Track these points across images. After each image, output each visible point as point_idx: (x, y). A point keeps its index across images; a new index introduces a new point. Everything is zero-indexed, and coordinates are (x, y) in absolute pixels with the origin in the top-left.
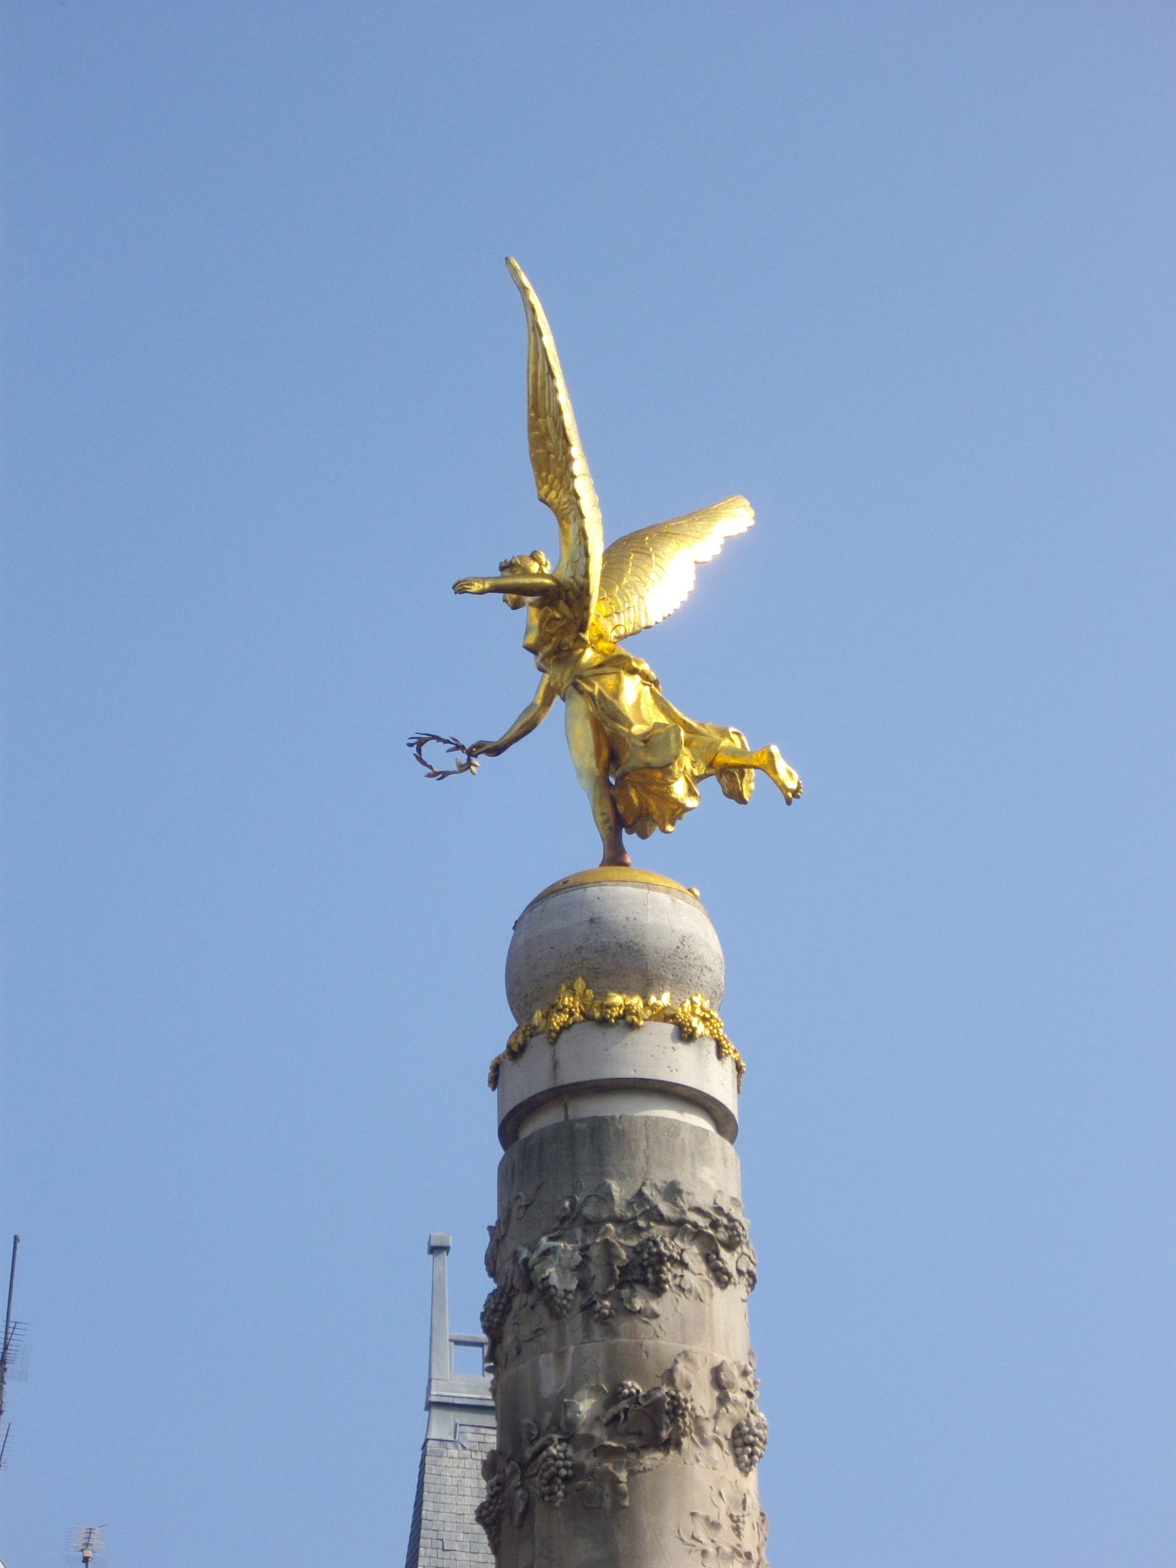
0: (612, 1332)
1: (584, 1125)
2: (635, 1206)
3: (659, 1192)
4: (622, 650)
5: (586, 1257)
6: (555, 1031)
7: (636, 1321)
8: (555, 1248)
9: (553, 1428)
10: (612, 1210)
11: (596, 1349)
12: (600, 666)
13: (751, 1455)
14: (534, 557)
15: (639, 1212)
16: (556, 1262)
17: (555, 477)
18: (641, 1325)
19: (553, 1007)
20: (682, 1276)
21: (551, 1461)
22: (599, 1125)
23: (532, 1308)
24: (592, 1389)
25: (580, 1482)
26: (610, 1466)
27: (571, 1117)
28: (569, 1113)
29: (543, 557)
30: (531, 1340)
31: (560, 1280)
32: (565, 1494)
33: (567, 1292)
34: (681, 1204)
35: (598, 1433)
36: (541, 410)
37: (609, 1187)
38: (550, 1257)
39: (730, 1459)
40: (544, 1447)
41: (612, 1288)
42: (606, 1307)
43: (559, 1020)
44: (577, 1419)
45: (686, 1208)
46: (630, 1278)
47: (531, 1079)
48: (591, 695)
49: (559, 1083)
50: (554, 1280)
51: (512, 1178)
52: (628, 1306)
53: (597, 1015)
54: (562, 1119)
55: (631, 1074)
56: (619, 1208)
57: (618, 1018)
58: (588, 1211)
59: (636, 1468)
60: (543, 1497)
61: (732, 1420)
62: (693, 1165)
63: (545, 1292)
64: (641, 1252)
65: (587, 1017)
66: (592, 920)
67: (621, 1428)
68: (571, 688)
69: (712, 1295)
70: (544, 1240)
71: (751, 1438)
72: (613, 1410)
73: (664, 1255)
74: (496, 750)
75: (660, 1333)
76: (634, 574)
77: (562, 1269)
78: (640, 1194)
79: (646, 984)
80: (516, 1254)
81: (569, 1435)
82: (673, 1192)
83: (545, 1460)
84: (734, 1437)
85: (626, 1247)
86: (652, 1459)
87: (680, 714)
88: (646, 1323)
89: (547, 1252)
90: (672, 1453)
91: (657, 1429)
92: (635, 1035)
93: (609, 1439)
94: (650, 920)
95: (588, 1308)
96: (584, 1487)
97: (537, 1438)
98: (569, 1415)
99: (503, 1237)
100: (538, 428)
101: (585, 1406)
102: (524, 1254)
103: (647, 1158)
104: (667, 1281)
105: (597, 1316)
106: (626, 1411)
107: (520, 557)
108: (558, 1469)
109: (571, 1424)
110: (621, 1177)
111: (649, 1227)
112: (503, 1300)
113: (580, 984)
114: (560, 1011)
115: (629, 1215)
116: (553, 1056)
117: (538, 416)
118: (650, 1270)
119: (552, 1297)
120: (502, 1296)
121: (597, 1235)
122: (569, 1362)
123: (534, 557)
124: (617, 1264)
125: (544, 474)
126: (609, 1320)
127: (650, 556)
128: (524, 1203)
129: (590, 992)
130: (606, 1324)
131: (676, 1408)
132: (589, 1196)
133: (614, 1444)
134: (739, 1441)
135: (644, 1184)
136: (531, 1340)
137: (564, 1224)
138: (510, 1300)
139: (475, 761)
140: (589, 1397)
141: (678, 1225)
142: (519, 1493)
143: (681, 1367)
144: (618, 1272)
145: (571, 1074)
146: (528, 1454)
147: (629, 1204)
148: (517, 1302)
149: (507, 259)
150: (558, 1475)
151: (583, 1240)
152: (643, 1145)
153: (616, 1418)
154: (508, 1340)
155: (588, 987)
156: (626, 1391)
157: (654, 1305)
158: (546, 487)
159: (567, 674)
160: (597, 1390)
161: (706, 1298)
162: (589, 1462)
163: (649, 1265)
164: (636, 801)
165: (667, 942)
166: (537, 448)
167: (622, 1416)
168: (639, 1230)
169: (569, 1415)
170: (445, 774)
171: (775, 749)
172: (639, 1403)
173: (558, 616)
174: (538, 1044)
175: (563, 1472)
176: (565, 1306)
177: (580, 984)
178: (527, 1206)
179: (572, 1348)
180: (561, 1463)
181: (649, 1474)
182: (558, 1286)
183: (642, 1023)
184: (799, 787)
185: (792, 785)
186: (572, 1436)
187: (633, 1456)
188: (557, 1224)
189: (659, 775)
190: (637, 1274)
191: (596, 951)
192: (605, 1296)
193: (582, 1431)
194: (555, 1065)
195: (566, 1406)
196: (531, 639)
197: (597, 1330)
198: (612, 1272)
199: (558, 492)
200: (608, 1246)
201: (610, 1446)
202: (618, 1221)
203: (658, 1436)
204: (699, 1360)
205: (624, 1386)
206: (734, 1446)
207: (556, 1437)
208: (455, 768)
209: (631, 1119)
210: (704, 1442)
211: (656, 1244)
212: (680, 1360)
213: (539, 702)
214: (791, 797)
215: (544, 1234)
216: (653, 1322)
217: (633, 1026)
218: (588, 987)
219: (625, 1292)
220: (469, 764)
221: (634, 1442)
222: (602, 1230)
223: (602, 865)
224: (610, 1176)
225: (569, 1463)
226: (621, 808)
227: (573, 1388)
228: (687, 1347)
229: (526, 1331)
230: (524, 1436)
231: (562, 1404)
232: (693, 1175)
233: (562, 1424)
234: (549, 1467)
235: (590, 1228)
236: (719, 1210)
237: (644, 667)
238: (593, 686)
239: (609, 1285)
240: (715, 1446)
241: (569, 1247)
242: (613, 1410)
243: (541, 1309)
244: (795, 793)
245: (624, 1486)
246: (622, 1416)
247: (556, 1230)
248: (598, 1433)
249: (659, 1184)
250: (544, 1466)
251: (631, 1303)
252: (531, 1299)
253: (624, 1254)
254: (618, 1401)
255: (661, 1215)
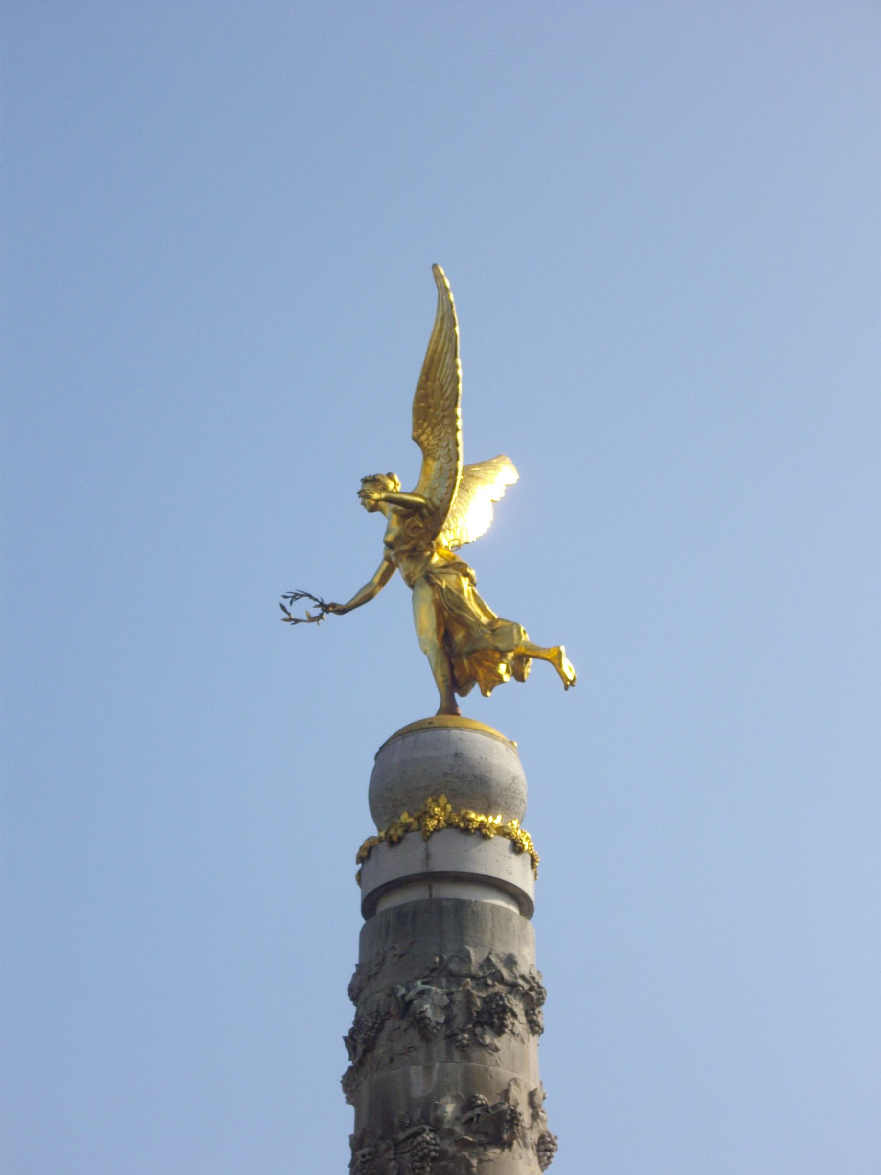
0: (467, 1058)
1: (449, 904)
2: (485, 968)
3: (501, 960)
4: (460, 558)
5: (452, 1001)
6: (429, 831)
7: (484, 1052)
8: (429, 990)
9: (423, 1121)
10: (470, 969)
11: (456, 1068)
12: (445, 567)
13: (549, 1158)
14: (390, 476)
15: (488, 973)
16: (430, 1001)
17: (428, 426)
18: (488, 1055)
19: (425, 813)
20: (513, 1024)
21: (425, 1145)
22: (460, 906)
23: (405, 1030)
24: (454, 1097)
25: (443, 1163)
26: (467, 1154)
27: (434, 896)
28: (434, 893)
29: (396, 478)
30: (403, 1054)
31: (433, 1015)
32: (432, 1169)
33: (437, 1023)
34: (515, 971)
35: (458, 1129)
36: (431, 377)
37: (468, 952)
38: (425, 996)
39: (536, 1159)
40: (416, 1135)
41: (470, 1026)
42: (465, 1039)
43: (432, 824)
44: (443, 1118)
45: (518, 975)
46: (482, 1020)
47: (395, 864)
48: (441, 587)
49: (430, 870)
50: (429, 1014)
51: (387, 933)
52: (481, 1040)
53: (462, 825)
54: (427, 897)
55: (483, 872)
56: (474, 969)
57: (476, 829)
58: (453, 967)
59: (484, 1158)
60: (414, 1169)
61: (539, 1131)
62: (519, 944)
63: (420, 1022)
64: (491, 1002)
65: (450, 825)
66: (456, 755)
67: (474, 1127)
68: (423, 580)
69: (529, 1040)
70: (419, 982)
71: (551, 1146)
72: (469, 1114)
73: (507, 1007)
74: (342, 611)
75: (500, 1063)
76: (460, 503)
77: (434, 1006)
78: (488, 960)
79: (488, 808)
80: (393, 992)
81: (437, 1126)
82: (511, 961)
83: (419, 1144)
84: (539, 1144)
85: (479, 997)
86: (494, 1152)
87: (490, 611)
88: (491, 1054)
89: (422, 993)
90: (506, 1150)
91: (499, 1133)
92: (485, 844)
93: (467, 1134)
94: (495, 761)
95: (451, 1038)
96: (446, 1167)
97: (409, 1127)
98: (439, 1113)
99: (375, 974)
100: (425, 389)
101: (450, 1108)
102: (402, 991)
103: (493, 935)
104: (506, 1026)
105: (458, 1044)
106: (478, 1115)
107: (382, 476)
108: (430, 1151)
109: (439, 1120)
110: (475, 946)
111: (494, 985)
112: (379, 1021)
113: (443, 800)
114: (432, 817)
115: (481, 974)
116: (426, 849)
117: (427, 380)
118: (496, 1016)
119: (426, 1026)
120: (377, 1018)
121: (460, 986)
122: (435, 1075)
123: (390, 476)
124: (474, 1008)
125: (421, 421)
126: (466, 1049)
127: (467, 491)
128: (399, 952)
129: (449, 807)
130: (464, 1051)
131: (513, 1118)
132: (452, 956)
133: (471, 1139)
134: (542, 1147)
135: (490, 953)
136: (403, 1054)
137: (434, 973)
138: (383, 1022)
139: (325, 615)
140: (452, 1103)
141: (513, 987)
142: (393, 1164)
143: (513, 1088)
144: (475, 1014)
145: (440, 865)
146: (401, 1136)
147: (481, 967)
148: (389, 1024)
149: (435, 267)
150: (428, 1155)
151: (448, 988)
152: (490, 924)
153: (470, 1120)
154: (380, 1051)
155: (448, 802)
156: (479, 1102)
157: (497, 1042)
158: (420, 431)
159: (419, 568)
160: (456, 1098)
161: (526, 1041)
162: (452, 1150)
163: (495, 1013)
164: (467, 669)
165: (506, 780)
166: (421, 402)
167: (475, 1119)
168: (487, 986)
169: (439, 1113)
170: (296, 621)
171: (563, 649)
172: (488, 1112)
173: (421, 525)
174: (413, 840)
175: (433, 1154)
176: (434, 1033)
177: (443, 800)
178: (401, 956)
179: (437, 1065)
180: (432, 1147)
181: (491, 1163)
182: (432, 1018)
183: (492, 836)
184: (574, 679)
185: (571, 677)
186: (439, 1129)
187: (481, 1149)
188: (427, 973)
189: (497, 655)
190: (486, 1018)
191: (458, 778)
192: (463, 1031)
193: (446, 1126)
194: (428, 856)
195: (436, 1107)
196: (390, 538)
197: (457, 1055)
198: (471, 1014)
199: (428, 436)
200: (468, 995)
201: (467, 1140)
202: (473, 977)
203: (501, 1138)
204: (522, 1084)
205: (477, 1098)
206: (538, 1150)
207: (427, 1128)
208: (305, 618)
209: (483, 904)
210: (525, 1145)
211: (502, 998)
212: (512, 1084)
213: (376, 580)
214: (569, 684)
215: (417, 978)
216: (496, 1054)
217: (485, 837)
218: (448, 802)
219: (478, 1030)
220: (320, 617)
221: (483, 1139)
222: (464, 983)
223: (438, 713)
224: (467, 943)
225: (437, 1148)
226: (457, 673)
227: (440, 1091)
228: (516, 1075)
229: (398, 1046)
230: (396, 1120)
231: (430, 1105)
232: (519, 951)
233: (431, 1119)
234: (422, 1149)
235: (453, 979)
236: (533, 978)
237: (472, 572)
238: (442, 581)
239: (468, 1022)
240: (530, 1150)
241: (439, 991)
242: (469, 1114)
243: (413, 1033)
244: (572, 683)
245: (474, 1169)
246: (475, 1119)
247: (426, 977)
248: (458, 1129)
249: (501, 955)
250: (419, 1147)
251: (483, 1038)
252: (404, 1024)
253: (479, 1002)
254: (472, 1109)
255: (502, 977)
